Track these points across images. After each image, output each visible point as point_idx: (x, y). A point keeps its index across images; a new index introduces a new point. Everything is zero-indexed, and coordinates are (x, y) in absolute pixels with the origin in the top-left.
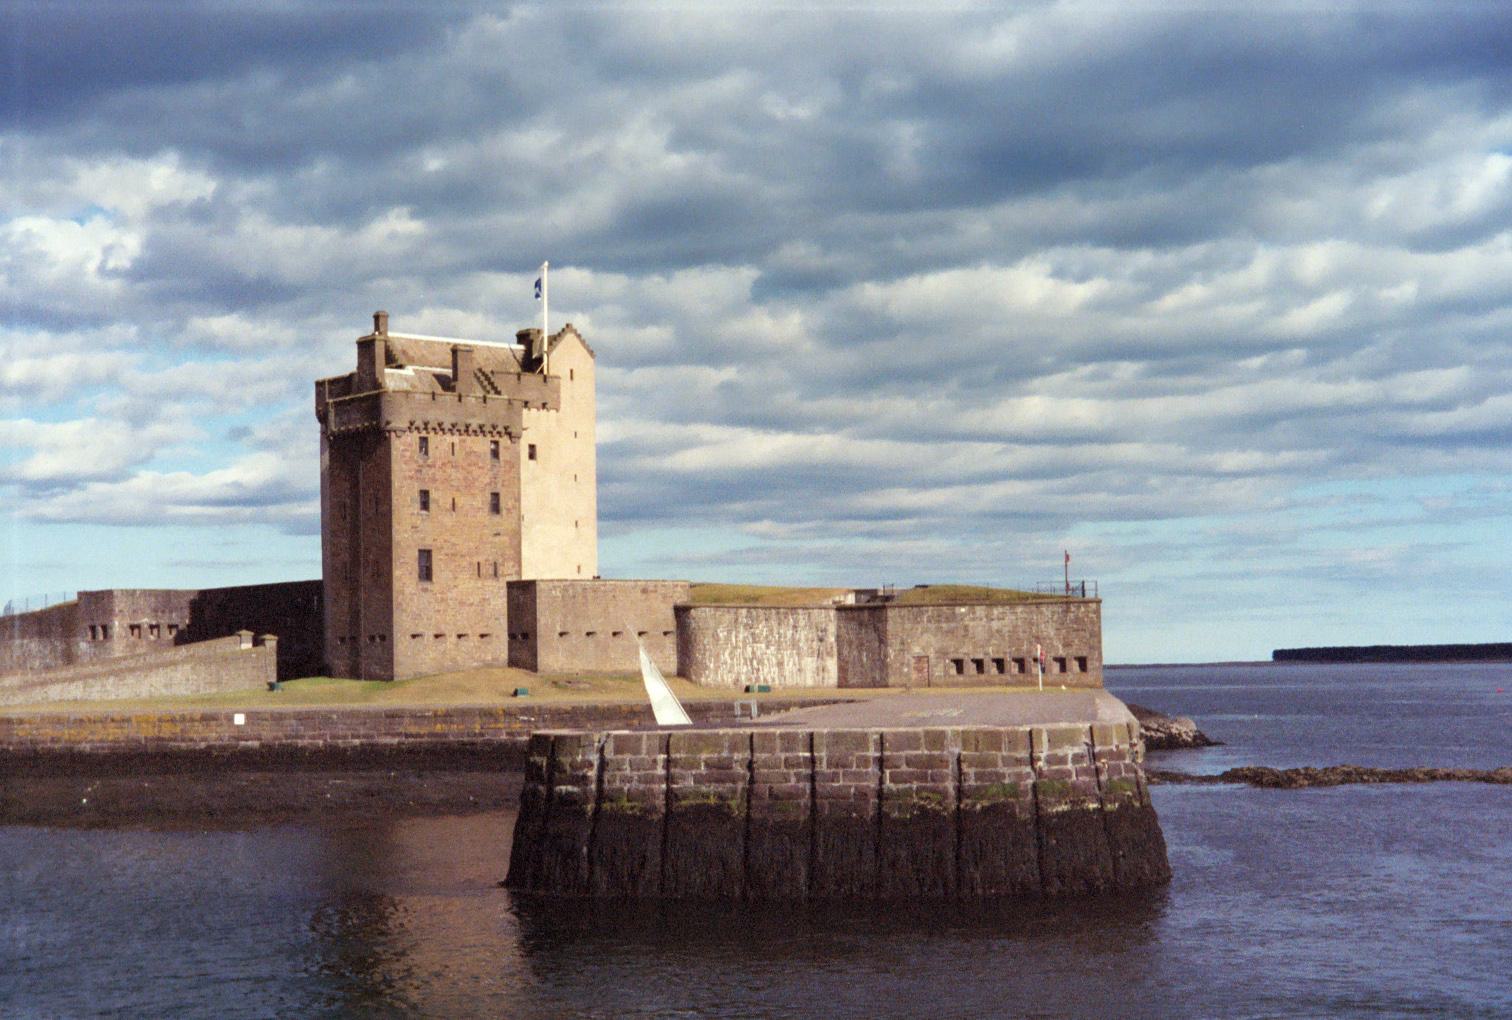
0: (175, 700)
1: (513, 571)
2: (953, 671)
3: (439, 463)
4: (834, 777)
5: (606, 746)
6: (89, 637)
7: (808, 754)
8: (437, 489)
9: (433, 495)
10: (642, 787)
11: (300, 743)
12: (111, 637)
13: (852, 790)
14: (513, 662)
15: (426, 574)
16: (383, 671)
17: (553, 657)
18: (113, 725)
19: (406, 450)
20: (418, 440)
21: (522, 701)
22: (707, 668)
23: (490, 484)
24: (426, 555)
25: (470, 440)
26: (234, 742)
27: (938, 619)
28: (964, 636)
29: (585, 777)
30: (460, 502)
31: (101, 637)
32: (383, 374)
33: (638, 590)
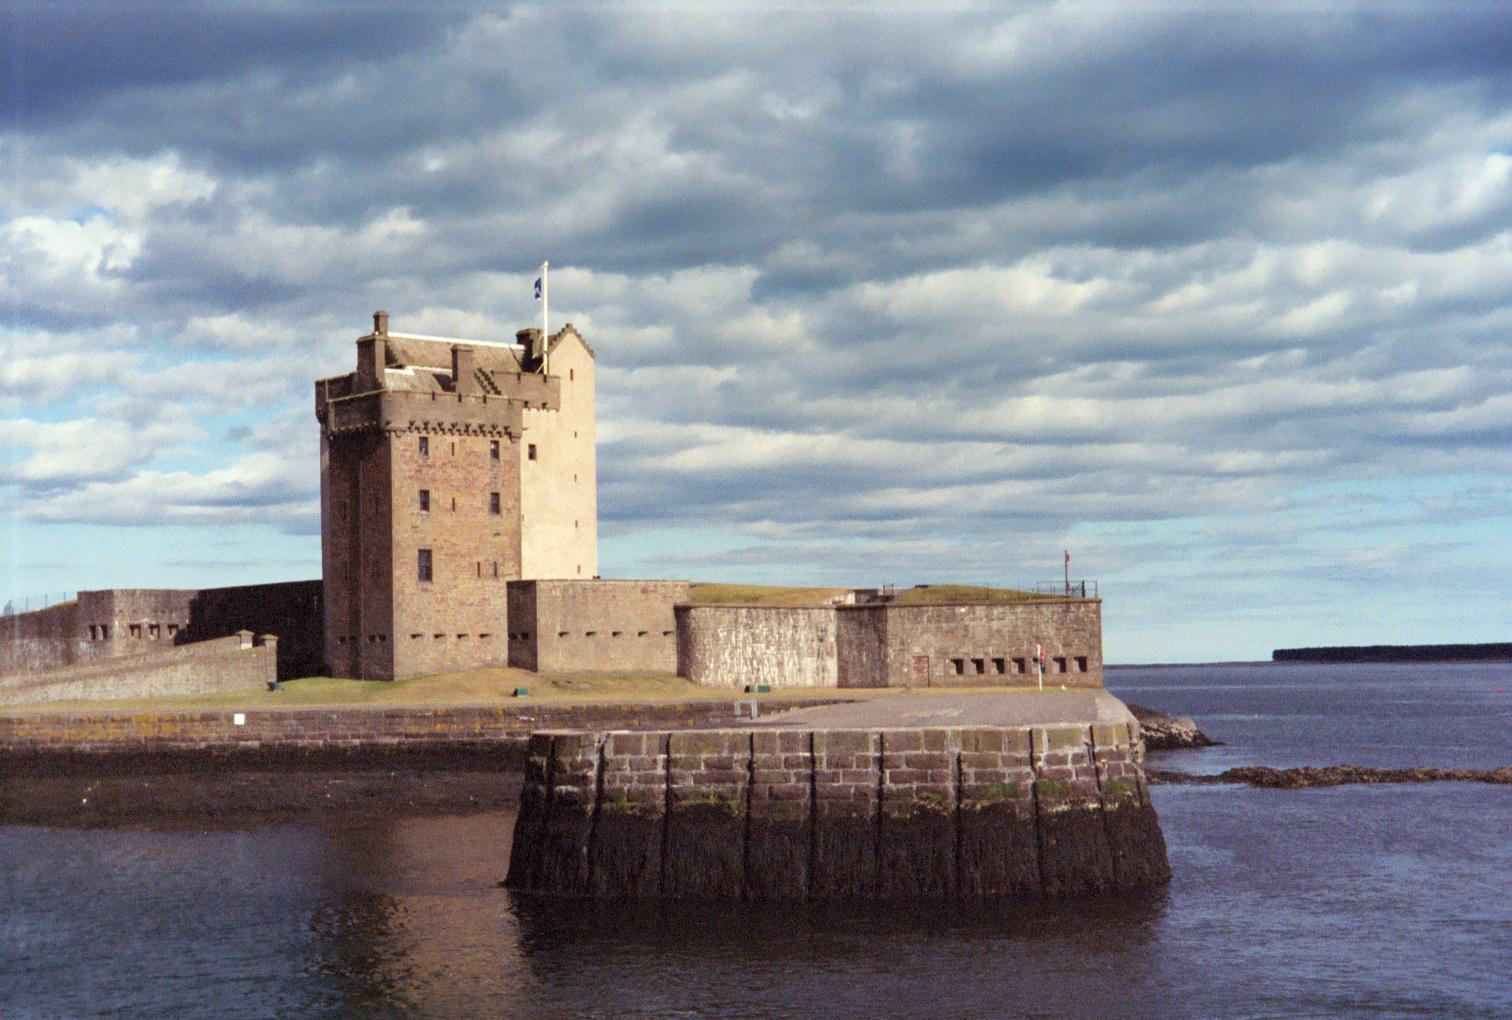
0: (175, 700)
1: (513, 571)
2: (953, 671)
3: (439, 463)
4: (834, 777)
5: (606, 746)
6: (89, 637)
7: (808, 754)
8: (437, 489)
9: (433, 495)
10: (642, 787)
11: (300, 743)
12: (111, 637)
13: (852, 790)
14: (513, 662)
15: (426, 574)
16: (383, 671)
17: (553, 657)
18: (113, 725)
19: (406, 450)
20: (418, 440)
21: (522, 701)
22: (707, 668)
23: (490, 484)
24: (426, 555)
25: (470, 440)
26: (234, 742)
27: (938, 619)
28: (964, 636)
29: (585, 777)
30: (460, 502)
31: (101, 637)
32: (383, 374)
33: (638, 590)
